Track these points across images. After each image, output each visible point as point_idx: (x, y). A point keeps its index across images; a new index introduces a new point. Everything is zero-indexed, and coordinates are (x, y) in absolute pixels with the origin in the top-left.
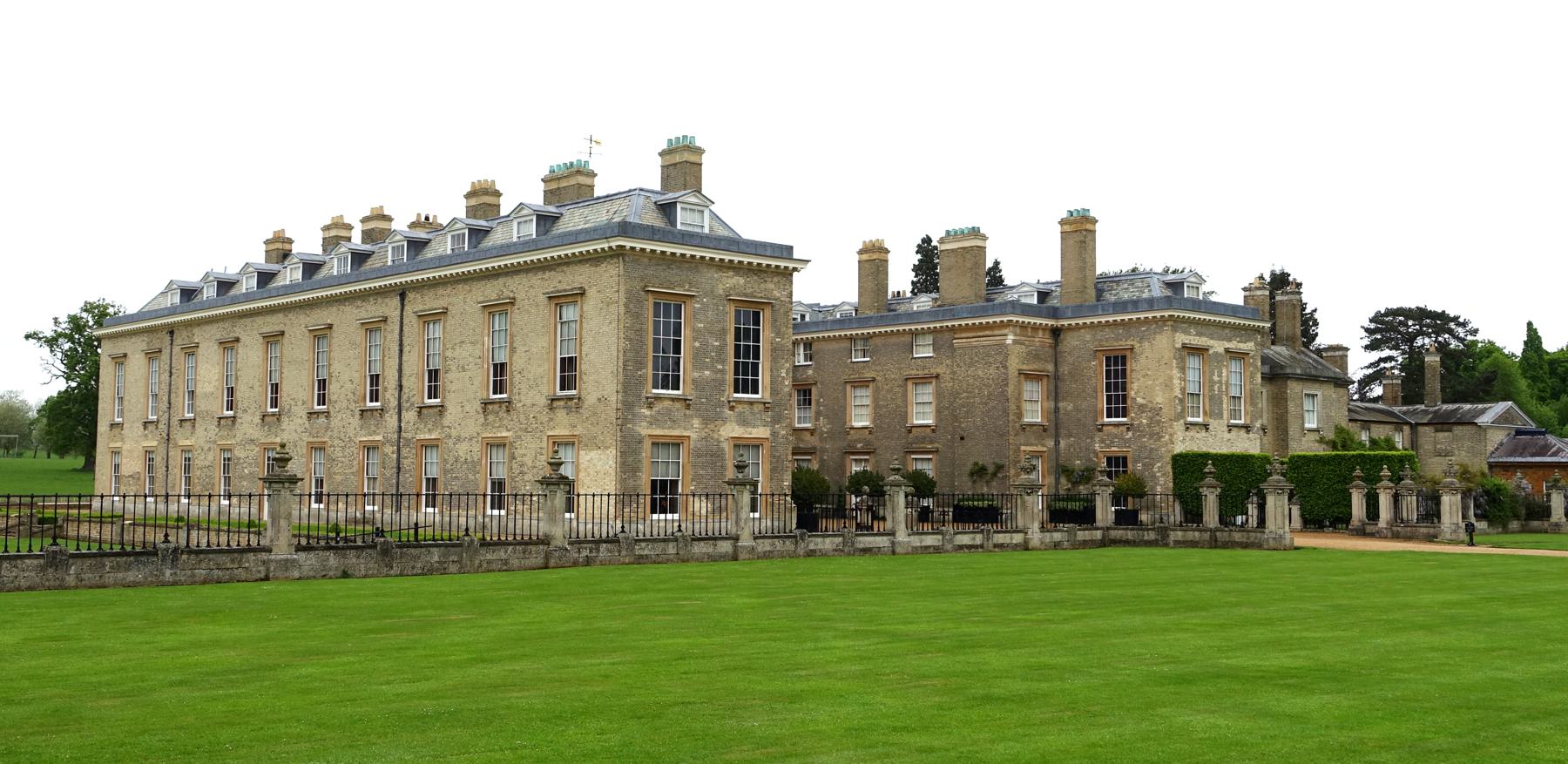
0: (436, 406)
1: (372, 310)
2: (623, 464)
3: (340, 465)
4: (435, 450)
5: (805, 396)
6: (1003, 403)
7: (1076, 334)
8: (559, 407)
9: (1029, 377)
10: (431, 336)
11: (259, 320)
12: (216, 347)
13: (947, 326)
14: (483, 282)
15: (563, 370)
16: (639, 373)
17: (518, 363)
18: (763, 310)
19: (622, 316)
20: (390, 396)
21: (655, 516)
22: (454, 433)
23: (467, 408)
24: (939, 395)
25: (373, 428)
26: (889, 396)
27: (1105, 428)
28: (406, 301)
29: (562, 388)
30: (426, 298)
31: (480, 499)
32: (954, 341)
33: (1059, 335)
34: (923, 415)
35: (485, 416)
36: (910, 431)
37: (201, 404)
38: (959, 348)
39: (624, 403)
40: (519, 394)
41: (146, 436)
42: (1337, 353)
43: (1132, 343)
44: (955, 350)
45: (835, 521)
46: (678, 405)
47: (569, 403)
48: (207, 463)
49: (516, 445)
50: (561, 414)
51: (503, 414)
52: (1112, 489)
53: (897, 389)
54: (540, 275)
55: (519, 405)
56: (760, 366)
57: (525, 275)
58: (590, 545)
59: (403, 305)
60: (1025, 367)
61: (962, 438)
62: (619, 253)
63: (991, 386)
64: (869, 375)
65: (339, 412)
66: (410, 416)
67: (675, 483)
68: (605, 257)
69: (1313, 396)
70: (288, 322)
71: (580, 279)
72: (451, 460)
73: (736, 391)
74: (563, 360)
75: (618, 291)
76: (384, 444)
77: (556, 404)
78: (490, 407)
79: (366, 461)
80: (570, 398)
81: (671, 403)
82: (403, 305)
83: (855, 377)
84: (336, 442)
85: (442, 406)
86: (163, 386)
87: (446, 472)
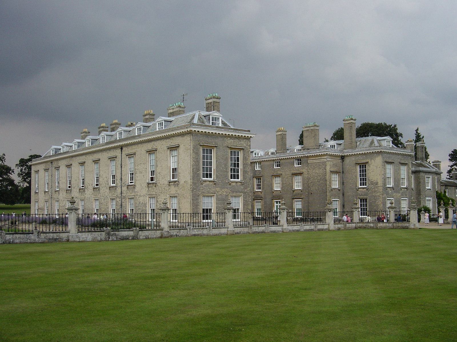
0: (133, 185)
1: (112, 154)
2: (193, 203)
3: (103, 205)
4: (133, 199)
5: (259, 180)
6: (324, 182)
7: (349, 158)
8: (172, 185)
9: (332, 172)
10: (152, 165)
11: (78, 158)
12: (65, 167)
13: (306, 156)
14: (147, 144)
15: (173, 172)
16: (198, 173)
17: (159, 170)
18: (240, 151)
19: (192, 154)
20: (118, 182)
21: (204, 221)
22: (139, 194)
23: (143, 186)
24: (303, 180)
25: (113, 193)
26: (287, 180)
27: (359, 189)
28: (123, 151)
29: (173, 178)
30: (129, 149)
31: (147, 215)
32: (308, 161)
33: (344, 158)
34: (297, 185)
35: (148, 188)
36: (294, 192)
37: (61, 186)
38: (310, 163)
39: (193, 183)
40: (159, 181)
41: (45, 196)
42: (437, 163)
43: (368, 160)
44: (308, 164)
45: (258, 221)
46: (211, 183)
47: (175, 183)
48: (63, 205)
49: (158, 198)
50: (173, 187)
51: (154, 187)
52: (445, 209)
53: (289, 178)
54: (165, 140)
55: (159, 184)
56: (212, 168)
57: (160, 141)
58: (177, 231)
59: (122, 152)
60: (332, 169)
61: (311, 194)
62: (190, 133)
63: (320, 176)
64: (279, 173)
65: (102, 187)
66: (124, 188)
67: (211, 210)
68: (186, 134)
69: (429, 177)
70: (87, 159)
71: (178, 141)
72: (138, 203)
73: (231, 178)
74: (173, 169)
75: (190, 145)
76: (116, 198)
77: (171, 184)
78: (150, 185)
79: (171, 203)
80: (175, 182)
81: (209, 182)
82: (122, 152)
83: (275, 174)
84: (102, 197)
85: (135, 185)
86: (50, 180)
87: (136, 207)
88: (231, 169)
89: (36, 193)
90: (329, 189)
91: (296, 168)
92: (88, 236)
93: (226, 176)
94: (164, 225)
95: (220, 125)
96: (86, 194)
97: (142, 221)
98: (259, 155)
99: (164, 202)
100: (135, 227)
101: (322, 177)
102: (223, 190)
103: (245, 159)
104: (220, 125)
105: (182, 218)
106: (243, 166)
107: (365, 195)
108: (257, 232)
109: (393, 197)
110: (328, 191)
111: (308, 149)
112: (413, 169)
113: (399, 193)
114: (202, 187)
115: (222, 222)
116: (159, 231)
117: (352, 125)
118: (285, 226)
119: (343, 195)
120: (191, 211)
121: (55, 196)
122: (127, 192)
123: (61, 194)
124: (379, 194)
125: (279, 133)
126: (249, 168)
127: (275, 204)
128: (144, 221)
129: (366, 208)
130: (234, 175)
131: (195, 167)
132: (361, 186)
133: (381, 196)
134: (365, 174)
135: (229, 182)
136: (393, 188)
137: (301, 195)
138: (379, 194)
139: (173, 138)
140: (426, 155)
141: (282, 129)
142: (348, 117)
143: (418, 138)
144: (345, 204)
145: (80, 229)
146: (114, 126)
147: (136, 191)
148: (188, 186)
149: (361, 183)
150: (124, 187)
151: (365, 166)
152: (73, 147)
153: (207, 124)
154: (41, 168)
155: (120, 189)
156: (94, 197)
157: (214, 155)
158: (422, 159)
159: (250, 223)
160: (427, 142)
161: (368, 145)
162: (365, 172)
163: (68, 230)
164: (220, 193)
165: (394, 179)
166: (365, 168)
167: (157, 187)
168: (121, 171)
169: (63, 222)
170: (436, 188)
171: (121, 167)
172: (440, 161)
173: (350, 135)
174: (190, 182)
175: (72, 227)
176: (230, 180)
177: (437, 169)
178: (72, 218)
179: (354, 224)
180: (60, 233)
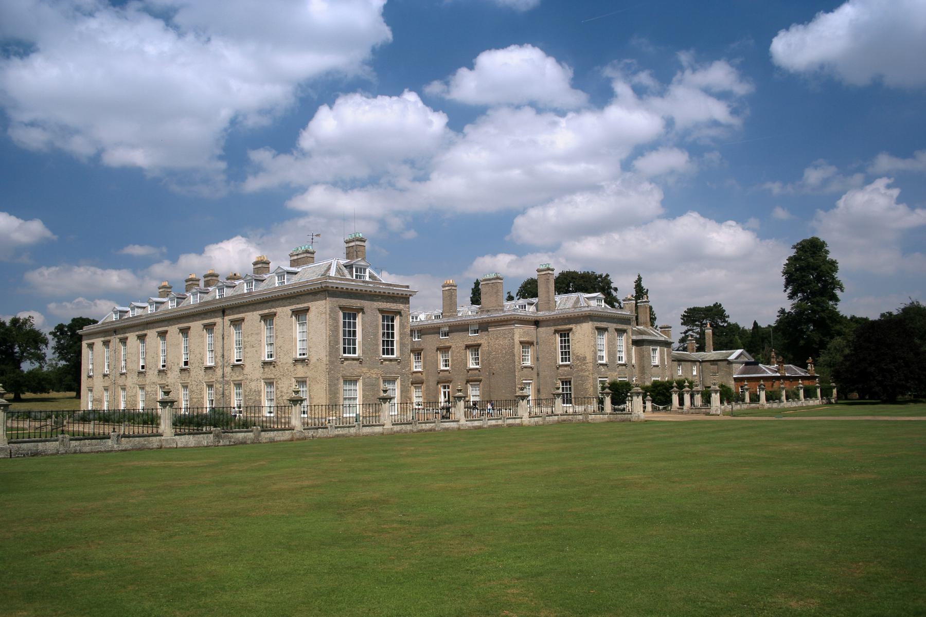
2: (330, 390)
3: (196, 394)
19: (328, 320)
23: (255, 365)
25: (211, 376)
33: (538, 324)
37: (130, 366)
41: (104, 381)
48: (133, 394)
61: (493, 374)
72: (248, 390)
73: (384, 354)
75: (325, 308)
84: (194, 383)
88: (383, 341)
89: (90, 377)
90: (518, 367)
91: (472, 338)
92: (189, 440)
93: (377, 350)
94: (296, 422)
95: (367, 279)
96: (168, 378)
97: (257, 417)
98: (418, 320)
99: (295, 390)
100: (255, 426)
101: (508, 350)
102: (372, 371)
103: (402, 326)
104: (367, 279)
105: (313, 412)
106: (400, 337)
107: (568, 375)
108: (423, 430)
109: (607, 377)
110: (517, 370)
111: (488, 311)
112: (634, 337)
113: (615, 372)
114: (343, 367)
115: (373, 416)
116: (289, 431)
117: (549, 277)
118: (463, 421)
119: (538, 374)
120: (328, 401)
121: (121, 381)
122: (232, 376)
123: (129, 379)
124: (587, 373)
125: (447, 288)
126: (408, 339)
127: (442, 390)
128: (252, 417)
129: (570, 394)
130: (388, 349)
131: (332, 338)
132: (563, 363)
133: (591, 376)
134: (569, 346)
135: (380, 359)
136: (607, 365)
137: (479, 376)
138: (587, 373)
139: (300, 297)
140: (651, 318)
141: (451, 282)
142: (544, 266)
143: (640, 292)
144: (541, 387)
145: (178, 430)
146: (209, 278)
147: (245, 372)
148: (323, 367)
149: (562, 358)
150: (226, 367)
151: (568, 334)
152: (149, 309)
153: (349, 277)
154: (98, 342)
155: (221, 370)
156: (181, 382)
157: (359, 320)
158: (645, 324)
159: (414, 418)
160: (653, 299)
161: (571, 305)
162: (569, 342)
163: (160, 431)
164: (368, 375)
165: (609, 351)
166: (568, 336)
167: (276, 367)
168: (223, 345)
169: (150, 419)
170: (666, 363)
171: (223, 338)
172: (670, 326)
173: (546, 289)
174: (325, 359)
175: (165, 426)
176: (381, 357)
177: (666, 337)
178: (165, 416)
179: (556, 417)
180: (149, 436)
